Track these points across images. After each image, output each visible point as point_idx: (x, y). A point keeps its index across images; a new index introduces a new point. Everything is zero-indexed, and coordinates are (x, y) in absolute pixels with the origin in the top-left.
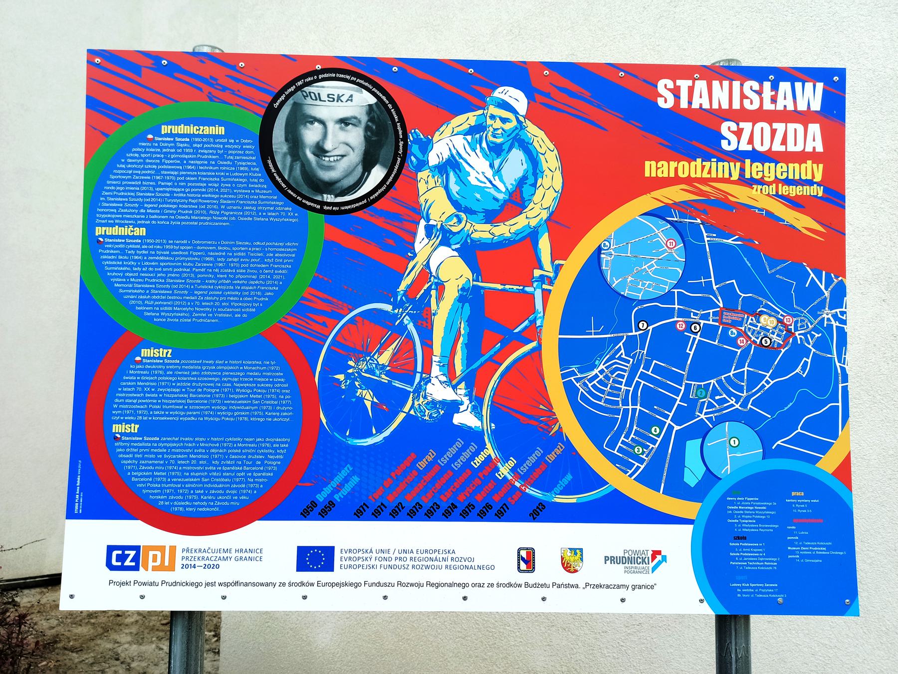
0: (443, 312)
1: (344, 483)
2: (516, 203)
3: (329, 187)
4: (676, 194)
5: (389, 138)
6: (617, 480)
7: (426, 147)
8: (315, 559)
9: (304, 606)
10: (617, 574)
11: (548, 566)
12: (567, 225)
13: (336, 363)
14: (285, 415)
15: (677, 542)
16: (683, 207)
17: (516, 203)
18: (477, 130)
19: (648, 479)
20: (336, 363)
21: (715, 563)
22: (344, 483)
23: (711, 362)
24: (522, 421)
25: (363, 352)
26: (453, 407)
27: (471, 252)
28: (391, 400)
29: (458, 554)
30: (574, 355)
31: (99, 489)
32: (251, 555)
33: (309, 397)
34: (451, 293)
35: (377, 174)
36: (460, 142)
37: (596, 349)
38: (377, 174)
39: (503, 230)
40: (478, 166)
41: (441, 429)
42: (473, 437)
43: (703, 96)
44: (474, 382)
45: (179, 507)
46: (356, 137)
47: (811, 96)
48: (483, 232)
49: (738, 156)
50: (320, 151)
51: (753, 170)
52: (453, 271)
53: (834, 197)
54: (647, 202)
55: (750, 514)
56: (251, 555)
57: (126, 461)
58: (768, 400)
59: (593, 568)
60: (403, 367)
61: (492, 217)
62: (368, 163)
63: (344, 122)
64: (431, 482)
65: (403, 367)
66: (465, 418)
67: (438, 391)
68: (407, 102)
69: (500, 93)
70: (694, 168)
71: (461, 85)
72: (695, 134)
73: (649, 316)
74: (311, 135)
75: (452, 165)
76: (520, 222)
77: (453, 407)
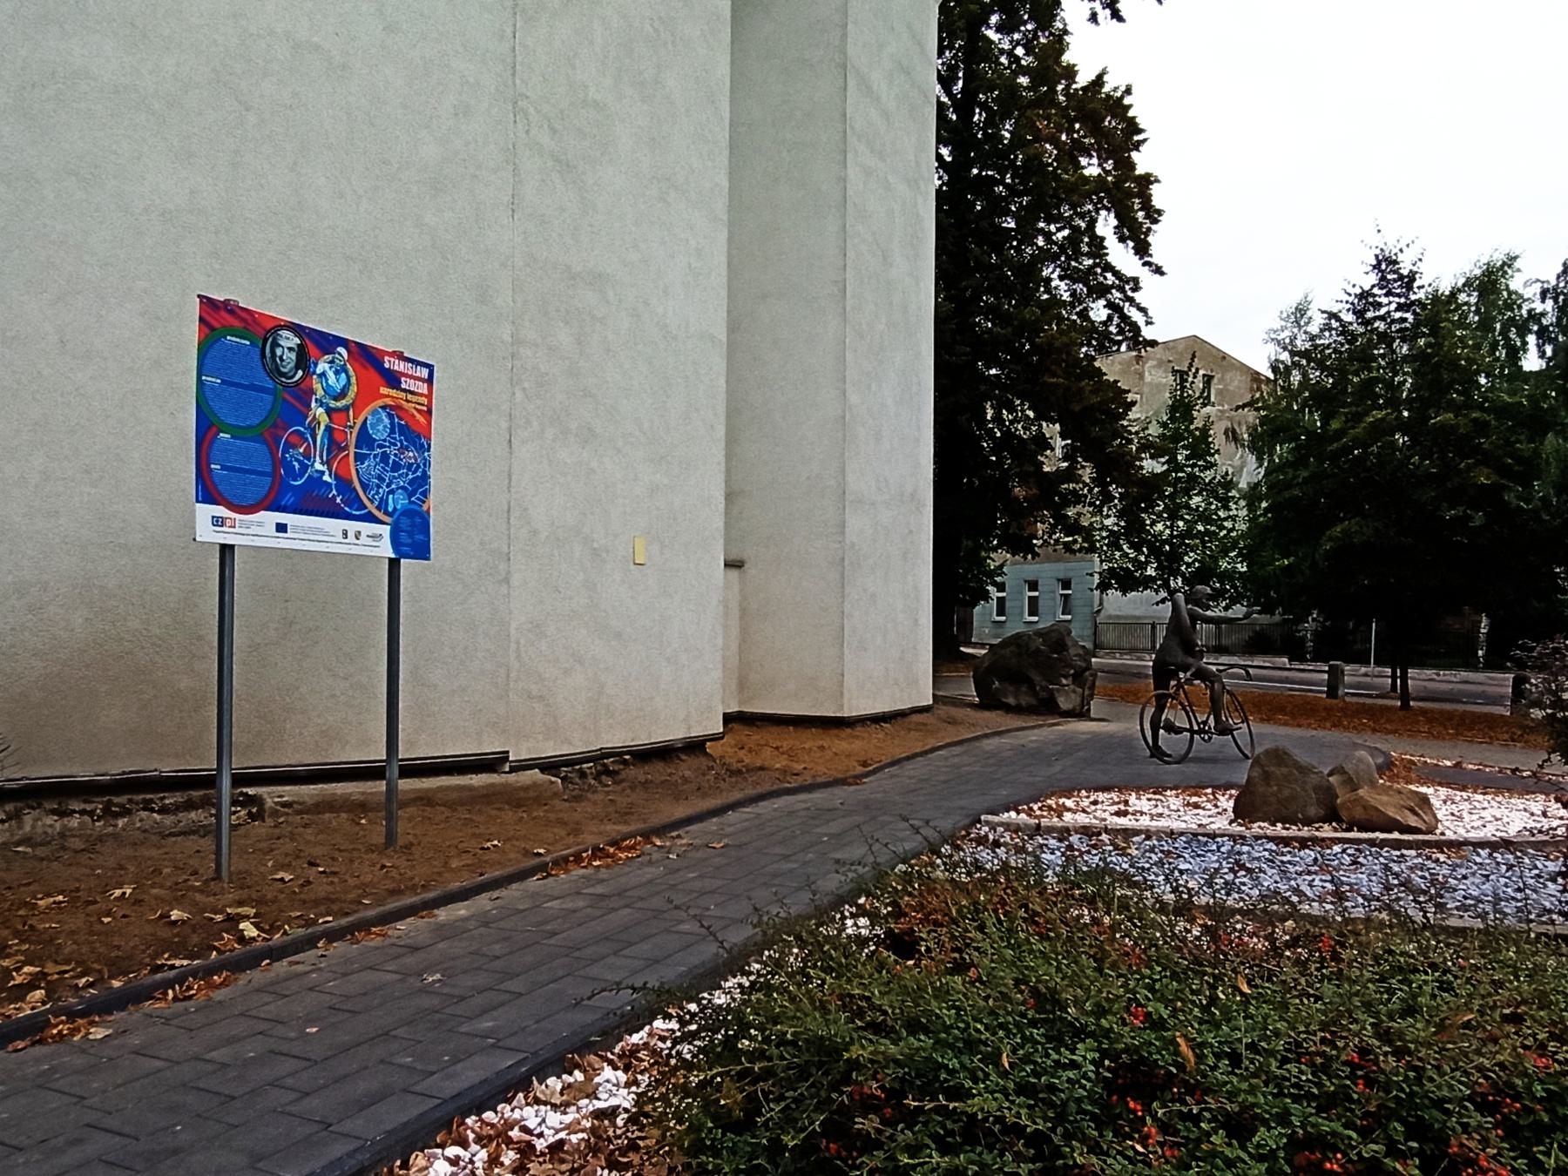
0: (320, 433)
1: (289, 499)
2: (343, 394)
3: (284, 375)
4: (389, 401)
5: (304, 360)
6: (372, 508)
7: (316, 365)
8: (281, 528)
9: (282, 542)
10: (370, 541)
11: (351, 535)
12: (357, 406)
13: (285, 451)
14: (269, 469)
15: (385, 530)
16: (391, 407)
17: (343, 394)
18: (332, 362)
19: (378, 508)
20: (285, 451)
21: (396, 542)
22: (289, 499)
23: (396, 467)
24: (344, 484)
25: (295, 447)
26: (323, 473)
27: (330, 412)
28: (304, 468)
29: (1138, 296)
30: (360, 458)
31: (208, 492)
32: (260, 524)
33: (278, 463)
34: (322, 427)
35: (300, 373)
36: (327, 366)
37: (366, 456)
38: (300, 373)
39: (339, 404)
40: (331, 375)
41: (317, 481)
42: (328, 485)
43: (400, 366)
44: (328, 463)
45: (236, 502)
46: (293, 356)
47: (425, 373)
48: (333, 404)
49: (405, 391)
50: (281, 359)
51: (410, 397)
52: (324, 420)
53: (430, 412)
54: (380, 402)
55: (405, 521)
56: (260, 524)
57: (216, 480)
58: (411, 482)
59: (363, 539)
60: (307, 455)
61: (336, 399)
62: (297, 367)
63: (290, 349)
64: (314, 502)
65: (307, 455)
66: (326, 478)
67: (318, 466)
68: (317, 342)
69: (340, 349)
70: (393, 392)
71: (327, 343)
72: (393, 379)
73: (381, 446)
74: (279, 352)
75: (323, 374)
76: (344, 402)
77: (323, 473)
